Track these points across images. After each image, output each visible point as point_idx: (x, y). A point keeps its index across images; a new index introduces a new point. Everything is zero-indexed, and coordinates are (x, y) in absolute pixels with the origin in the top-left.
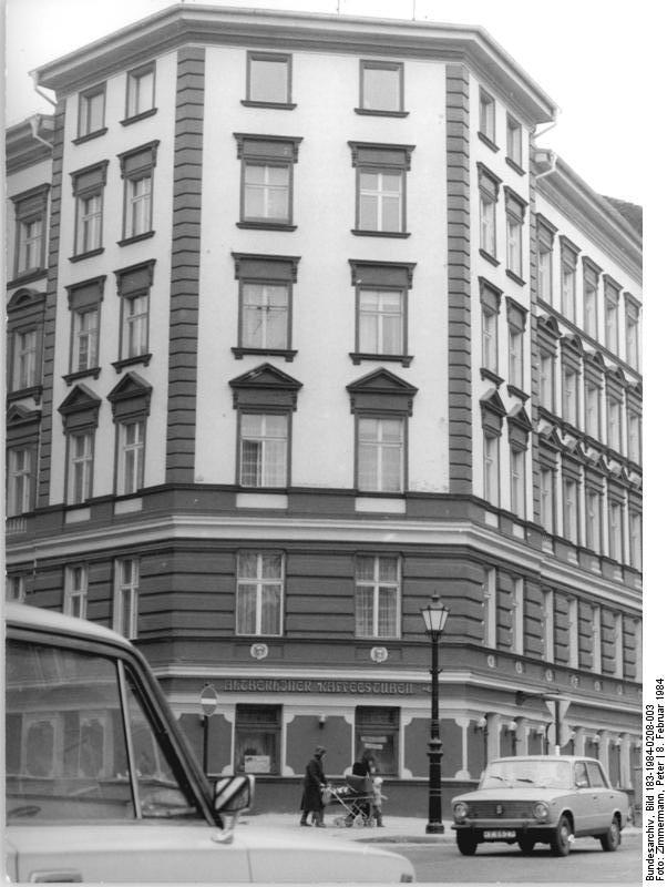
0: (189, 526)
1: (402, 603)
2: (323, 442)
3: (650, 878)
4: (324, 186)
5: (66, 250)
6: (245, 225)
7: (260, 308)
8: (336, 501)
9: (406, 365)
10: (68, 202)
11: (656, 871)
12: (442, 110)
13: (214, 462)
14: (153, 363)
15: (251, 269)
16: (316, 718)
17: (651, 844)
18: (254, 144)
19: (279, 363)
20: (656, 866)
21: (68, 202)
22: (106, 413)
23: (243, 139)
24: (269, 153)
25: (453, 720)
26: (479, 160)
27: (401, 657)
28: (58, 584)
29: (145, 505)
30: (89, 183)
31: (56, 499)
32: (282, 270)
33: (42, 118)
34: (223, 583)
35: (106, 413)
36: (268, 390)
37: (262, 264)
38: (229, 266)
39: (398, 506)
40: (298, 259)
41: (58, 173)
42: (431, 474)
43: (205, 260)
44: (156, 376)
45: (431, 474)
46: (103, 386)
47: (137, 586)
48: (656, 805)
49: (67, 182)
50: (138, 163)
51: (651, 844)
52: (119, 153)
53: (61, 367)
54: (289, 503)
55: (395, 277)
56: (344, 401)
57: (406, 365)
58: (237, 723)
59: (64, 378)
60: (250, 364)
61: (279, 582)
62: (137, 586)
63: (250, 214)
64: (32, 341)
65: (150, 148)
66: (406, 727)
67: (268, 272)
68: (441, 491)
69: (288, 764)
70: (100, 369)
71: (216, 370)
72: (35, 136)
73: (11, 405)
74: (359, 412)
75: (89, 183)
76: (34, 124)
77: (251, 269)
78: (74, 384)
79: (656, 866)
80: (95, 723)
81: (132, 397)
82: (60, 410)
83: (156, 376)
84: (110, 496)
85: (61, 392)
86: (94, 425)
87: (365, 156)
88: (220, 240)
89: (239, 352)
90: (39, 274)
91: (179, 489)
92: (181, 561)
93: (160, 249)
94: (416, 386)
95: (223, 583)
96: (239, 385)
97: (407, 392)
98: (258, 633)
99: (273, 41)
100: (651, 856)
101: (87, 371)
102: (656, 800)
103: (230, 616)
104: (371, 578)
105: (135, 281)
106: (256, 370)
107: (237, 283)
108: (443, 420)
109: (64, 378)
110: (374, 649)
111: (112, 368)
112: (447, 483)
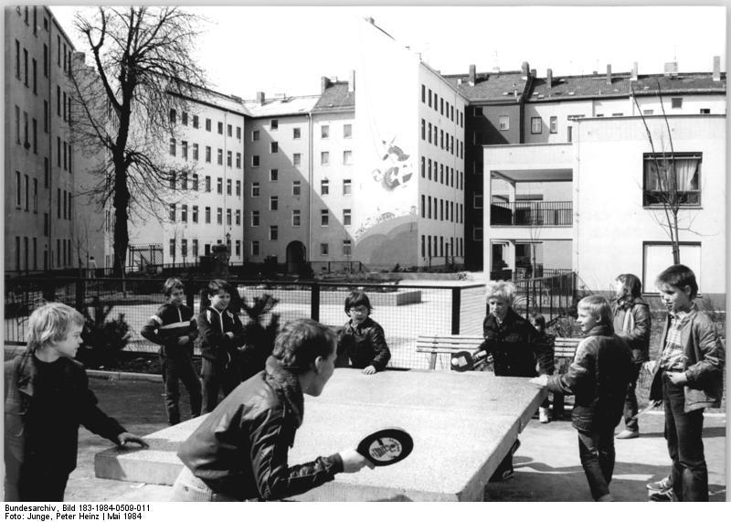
3: (7, 508)
11: (13, 513)
17: (36, 509)
20: (18, 513)
48: (69, 513)
51: (36, 509)
63: (566, 142)
79: (18, 513)
100: (26, 508)
102: (72, 513)
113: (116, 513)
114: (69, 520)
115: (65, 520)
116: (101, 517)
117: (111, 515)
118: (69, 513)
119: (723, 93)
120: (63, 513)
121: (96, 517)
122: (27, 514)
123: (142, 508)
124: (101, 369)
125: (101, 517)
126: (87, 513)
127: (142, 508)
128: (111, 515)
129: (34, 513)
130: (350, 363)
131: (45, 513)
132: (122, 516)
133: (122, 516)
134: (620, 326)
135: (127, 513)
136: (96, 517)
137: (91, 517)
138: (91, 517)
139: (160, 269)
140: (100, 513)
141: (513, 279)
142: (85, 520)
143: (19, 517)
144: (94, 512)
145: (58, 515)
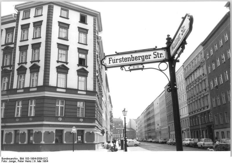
0: (47, 94)
1: (85, 111)
2: (73, 80)
4: (73, 33)
5: (19, 39)
6: (59, 38)
7: (61, 54)
8: (74, 91)
9: (87, 68)
10: (20, 30)
11: (4, 160)
12: (93, 25)
13: (52, 82)
14: (40, 62)
15: (60, 46)
16: (49, 132)
18: (62, 24)
19: (65, 64)
20: (6, 160)
21: (20, 30)
22: (28, 71)
23: (59, 23)
24: (64, 26)
25: (41, 131)
26: (182, 17)
27: (64, 120)
28: (27, 103)
29: (37, 89)
30: (25, 27)
31: (15, 87)
32: (66, 48)
33: (15, 14)
34: (53, 106)
35: (28, 71)
36: (63, 69)
37: (63, 46)
38: (56, 46)
39: (85, 93)
40: (69, 46)
41: (17, 25)
42: (90, 88)
43: (52, 44)
44: (42, 64)
45: (90, 88)
46: (28, 65)
47: (35, 105)
48: (22, 160)
49: (20, 27)
50: (38, 25)
52: (33, 22)
53: (17, 61)
54: (66, 91)
55: (86, 52)
56: (76, 73)
57: (87, 68)
58: (77, 133)
59: (18, 64)
60: (60, 64)
61: (64, 106)
62: (4, 108)
63: (60, 36)
64: (9, 57)
65: (13, 28)
66: (65, 133)
67: (63, 47)
68: (92, 90)
69: (65, 141)
70: (40, 60)
71: (54, 65)
72: (13, 17)
73: (4, 69)
74: (79, 75)
75: (25, 27)
76: (13, 15)
77: (60, 46)
78: (33, 63)
79: (6, 160)
80: (24, 132)
81: (35, 69)
82: (17, 70)
83: (42, 64)
84: (29, 87)
85: (17, 67)
86: (25, 73)
87: (81, 30)
88: (55, 40)
89: (58, 62)
90: (11, 43)
91: (46, 86)
92: (46, 101)
93: (43, 40)
94: (88, 71)
95: (53, 106)
96: (58, 68)
97: (87, 72)
98: (59, 115)
99: (66, 8)
101: (7, 66)
103: (54, 112)
104: (58, 107)
105: (36, 46)
106: (61, 65)
107: (58, 49)
108: (92, 78)
109: (18, 64)
110: (80, 119)
111: (30, 63)
112: (93, 89)
113: (40, 160)
114: (22, 162)
115: (21, 162)
116: (32, 161)
117: (38, 161)
118: (22, 160)
119: (2, 17)
120: (20, 160)
121: (31, 161)
122: (9, 160)
123: (45, 158)
124: (59, 121)
125: (32, 161)
126: (28, 160)
127: (45, 158)
128: (38, 161)
129: (11, 160)
130: (59, 105)
131: (14, 160)
132: (42, 161)
133: (42, 161)
134: (174, 46)
135: (44, 160)
136: (31, 161)
137: (29, 161)
138: (29, 161)
139: (175, 87)
140: (32, 160)
141: (204, 47)
142: (27, 162)
143: (6, 161)
144: (30, 160)
145: (18, 161)
